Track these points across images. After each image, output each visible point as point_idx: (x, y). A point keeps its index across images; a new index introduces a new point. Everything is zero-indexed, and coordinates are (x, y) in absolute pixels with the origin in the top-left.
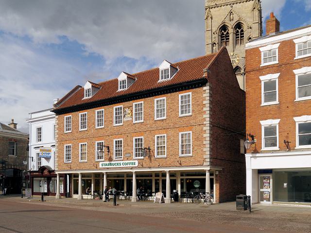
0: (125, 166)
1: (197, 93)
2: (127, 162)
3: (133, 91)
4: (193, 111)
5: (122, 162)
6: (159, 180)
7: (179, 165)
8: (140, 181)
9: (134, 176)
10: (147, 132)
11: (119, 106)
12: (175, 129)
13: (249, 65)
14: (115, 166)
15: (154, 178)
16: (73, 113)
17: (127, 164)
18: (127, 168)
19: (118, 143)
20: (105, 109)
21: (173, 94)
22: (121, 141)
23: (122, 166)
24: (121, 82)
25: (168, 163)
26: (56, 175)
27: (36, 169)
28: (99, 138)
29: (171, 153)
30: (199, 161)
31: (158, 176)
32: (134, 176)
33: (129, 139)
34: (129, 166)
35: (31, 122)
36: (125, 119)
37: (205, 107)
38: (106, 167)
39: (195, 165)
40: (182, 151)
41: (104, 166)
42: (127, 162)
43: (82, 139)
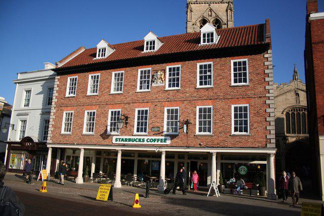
0: (150, 143)
1: (256, 60)
2: (154, 138)
3: (167, 52)
4: (251, 80)
5: (146, 138)
6: (100, 158)
7: (199, 146)
8: (230, 167)
9: (163, 157)
10: (185, 102)
11: (147, 69)
12: (226, 100)
13: (316, 36)
14: (135, 143)
15: (136, 159)
16: (103, 71)
17: (155, 140)
18: (153, 146)
19: (205, 113)
20: (126, 72)
21: (223, 59)
22: (146, 111)
23: (145, 143)
24: (100, 50)
25: (216, 142)
26: (48, 148)
27: (18, 140)
28: (114, 105)
29: (221, 129)
30: (261, 142)
31: (183, 158)
32: (163, 157)
33: (158, 109)
34: (156, 143)
35: (18, 83)
36: (154, 85)
37: (57, 90)
38: (122, 142)
39: (254, 146)
40: (138, 128)
41: (119, 141)
42: (154, 138)
43: (90, 105)
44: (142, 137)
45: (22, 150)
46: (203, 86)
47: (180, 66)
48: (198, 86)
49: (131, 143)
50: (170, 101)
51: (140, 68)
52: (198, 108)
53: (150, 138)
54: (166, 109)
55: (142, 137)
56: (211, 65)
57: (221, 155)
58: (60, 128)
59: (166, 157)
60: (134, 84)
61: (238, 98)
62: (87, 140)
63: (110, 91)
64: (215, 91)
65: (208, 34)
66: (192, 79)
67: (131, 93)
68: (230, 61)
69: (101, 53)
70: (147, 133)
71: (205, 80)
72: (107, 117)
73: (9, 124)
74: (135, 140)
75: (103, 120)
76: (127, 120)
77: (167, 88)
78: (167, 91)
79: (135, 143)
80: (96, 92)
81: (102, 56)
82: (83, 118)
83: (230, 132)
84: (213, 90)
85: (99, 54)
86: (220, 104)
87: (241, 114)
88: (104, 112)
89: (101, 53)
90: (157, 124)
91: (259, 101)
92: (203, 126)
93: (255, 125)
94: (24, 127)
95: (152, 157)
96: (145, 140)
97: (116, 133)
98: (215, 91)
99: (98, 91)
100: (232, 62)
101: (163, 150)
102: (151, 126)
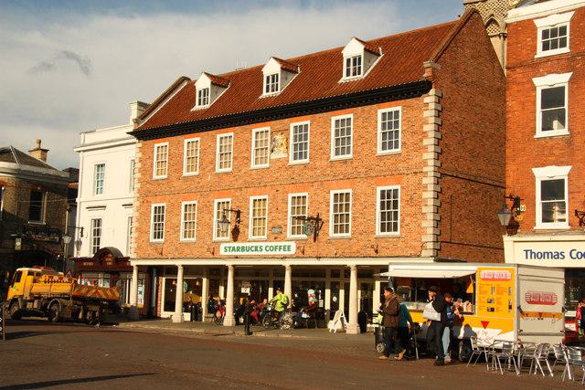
0: (270, 253)
2: (274, 244)
5: (264, 244)
9: (180, 272)
10: (315, 184)
11: (393, 109)
14: (250, 253)
16: (273, 122)
18: (273, 257)
21: (367, 108)
23: (264, 252)
25: (354, 249)
28: (221, 193)
29: (361, 228)
30: (414, 248)
32: (180, 272)
42: (274, 244)
44: (258, 244)
45: (98, 272)
46: (341, 157)
47: (308, 122)
48: (380, 152)
49: (245, 253)
50: (295, 184)
51: (379, 108)
52: (332, 193)
53: (269, 244)
54: (290, 196)
55: (258, 244)
56: (564, 87)
57: (332, 270)
58: (148, 232)
59: (293, 275)
60: (246, 155)
61: (384, 176)
62: (187, 251)
63: (151, 176)
64: (355, 164)
65: (355, 60)
66: (325, 145)
67: (243, 171)
68: (377, 112)
69: (352, 67)
70: (265, 237)
71: (390, 139)
72: (211, 212)
73: (75, 227)
74: (250, 249)
75: (207, 217)
76: (238, 216)
77: (292, 162)
78: (291, 167)
79: (250, 253)
80: (349, 153)
81: (273, 91)
82: (179, 215)
83: (373, 232)
84: (352, 163)
85: (268, 87)
86: (362, 186)
87: (389, 200)
88: (208, 204)
89: (270, 84)
90: (280, 223)
91: (413, 179)
92: (386, 222)
93: (408, 220)
94: (97, 232)
95: (312, 276)
96: (264, 248)
97: (225, 238)
98: (355, 164)
99: (400, 145)
100: (380, 112)
101: (287, 263)
102: (271, 225)
